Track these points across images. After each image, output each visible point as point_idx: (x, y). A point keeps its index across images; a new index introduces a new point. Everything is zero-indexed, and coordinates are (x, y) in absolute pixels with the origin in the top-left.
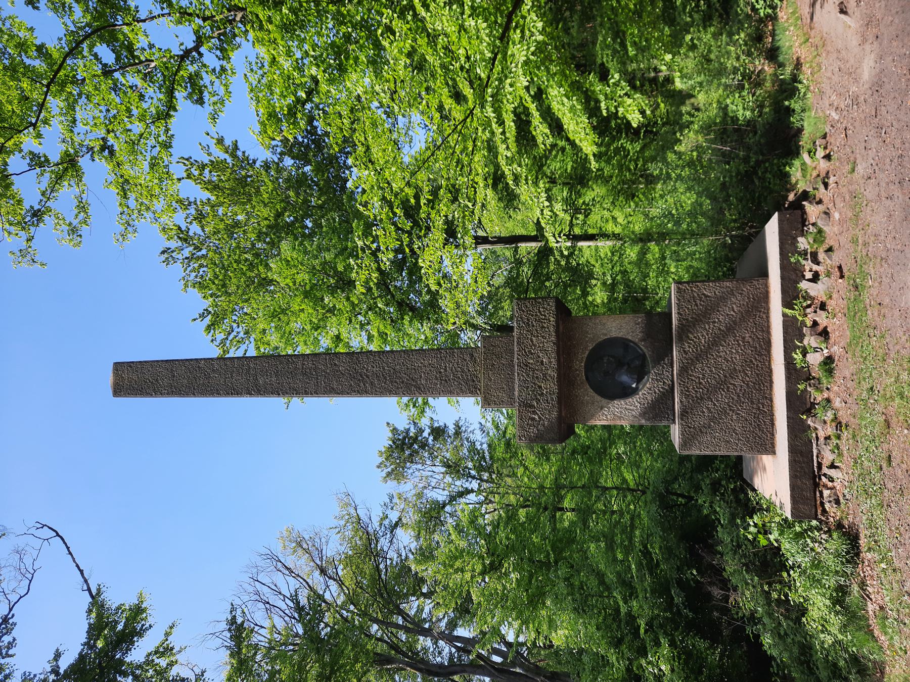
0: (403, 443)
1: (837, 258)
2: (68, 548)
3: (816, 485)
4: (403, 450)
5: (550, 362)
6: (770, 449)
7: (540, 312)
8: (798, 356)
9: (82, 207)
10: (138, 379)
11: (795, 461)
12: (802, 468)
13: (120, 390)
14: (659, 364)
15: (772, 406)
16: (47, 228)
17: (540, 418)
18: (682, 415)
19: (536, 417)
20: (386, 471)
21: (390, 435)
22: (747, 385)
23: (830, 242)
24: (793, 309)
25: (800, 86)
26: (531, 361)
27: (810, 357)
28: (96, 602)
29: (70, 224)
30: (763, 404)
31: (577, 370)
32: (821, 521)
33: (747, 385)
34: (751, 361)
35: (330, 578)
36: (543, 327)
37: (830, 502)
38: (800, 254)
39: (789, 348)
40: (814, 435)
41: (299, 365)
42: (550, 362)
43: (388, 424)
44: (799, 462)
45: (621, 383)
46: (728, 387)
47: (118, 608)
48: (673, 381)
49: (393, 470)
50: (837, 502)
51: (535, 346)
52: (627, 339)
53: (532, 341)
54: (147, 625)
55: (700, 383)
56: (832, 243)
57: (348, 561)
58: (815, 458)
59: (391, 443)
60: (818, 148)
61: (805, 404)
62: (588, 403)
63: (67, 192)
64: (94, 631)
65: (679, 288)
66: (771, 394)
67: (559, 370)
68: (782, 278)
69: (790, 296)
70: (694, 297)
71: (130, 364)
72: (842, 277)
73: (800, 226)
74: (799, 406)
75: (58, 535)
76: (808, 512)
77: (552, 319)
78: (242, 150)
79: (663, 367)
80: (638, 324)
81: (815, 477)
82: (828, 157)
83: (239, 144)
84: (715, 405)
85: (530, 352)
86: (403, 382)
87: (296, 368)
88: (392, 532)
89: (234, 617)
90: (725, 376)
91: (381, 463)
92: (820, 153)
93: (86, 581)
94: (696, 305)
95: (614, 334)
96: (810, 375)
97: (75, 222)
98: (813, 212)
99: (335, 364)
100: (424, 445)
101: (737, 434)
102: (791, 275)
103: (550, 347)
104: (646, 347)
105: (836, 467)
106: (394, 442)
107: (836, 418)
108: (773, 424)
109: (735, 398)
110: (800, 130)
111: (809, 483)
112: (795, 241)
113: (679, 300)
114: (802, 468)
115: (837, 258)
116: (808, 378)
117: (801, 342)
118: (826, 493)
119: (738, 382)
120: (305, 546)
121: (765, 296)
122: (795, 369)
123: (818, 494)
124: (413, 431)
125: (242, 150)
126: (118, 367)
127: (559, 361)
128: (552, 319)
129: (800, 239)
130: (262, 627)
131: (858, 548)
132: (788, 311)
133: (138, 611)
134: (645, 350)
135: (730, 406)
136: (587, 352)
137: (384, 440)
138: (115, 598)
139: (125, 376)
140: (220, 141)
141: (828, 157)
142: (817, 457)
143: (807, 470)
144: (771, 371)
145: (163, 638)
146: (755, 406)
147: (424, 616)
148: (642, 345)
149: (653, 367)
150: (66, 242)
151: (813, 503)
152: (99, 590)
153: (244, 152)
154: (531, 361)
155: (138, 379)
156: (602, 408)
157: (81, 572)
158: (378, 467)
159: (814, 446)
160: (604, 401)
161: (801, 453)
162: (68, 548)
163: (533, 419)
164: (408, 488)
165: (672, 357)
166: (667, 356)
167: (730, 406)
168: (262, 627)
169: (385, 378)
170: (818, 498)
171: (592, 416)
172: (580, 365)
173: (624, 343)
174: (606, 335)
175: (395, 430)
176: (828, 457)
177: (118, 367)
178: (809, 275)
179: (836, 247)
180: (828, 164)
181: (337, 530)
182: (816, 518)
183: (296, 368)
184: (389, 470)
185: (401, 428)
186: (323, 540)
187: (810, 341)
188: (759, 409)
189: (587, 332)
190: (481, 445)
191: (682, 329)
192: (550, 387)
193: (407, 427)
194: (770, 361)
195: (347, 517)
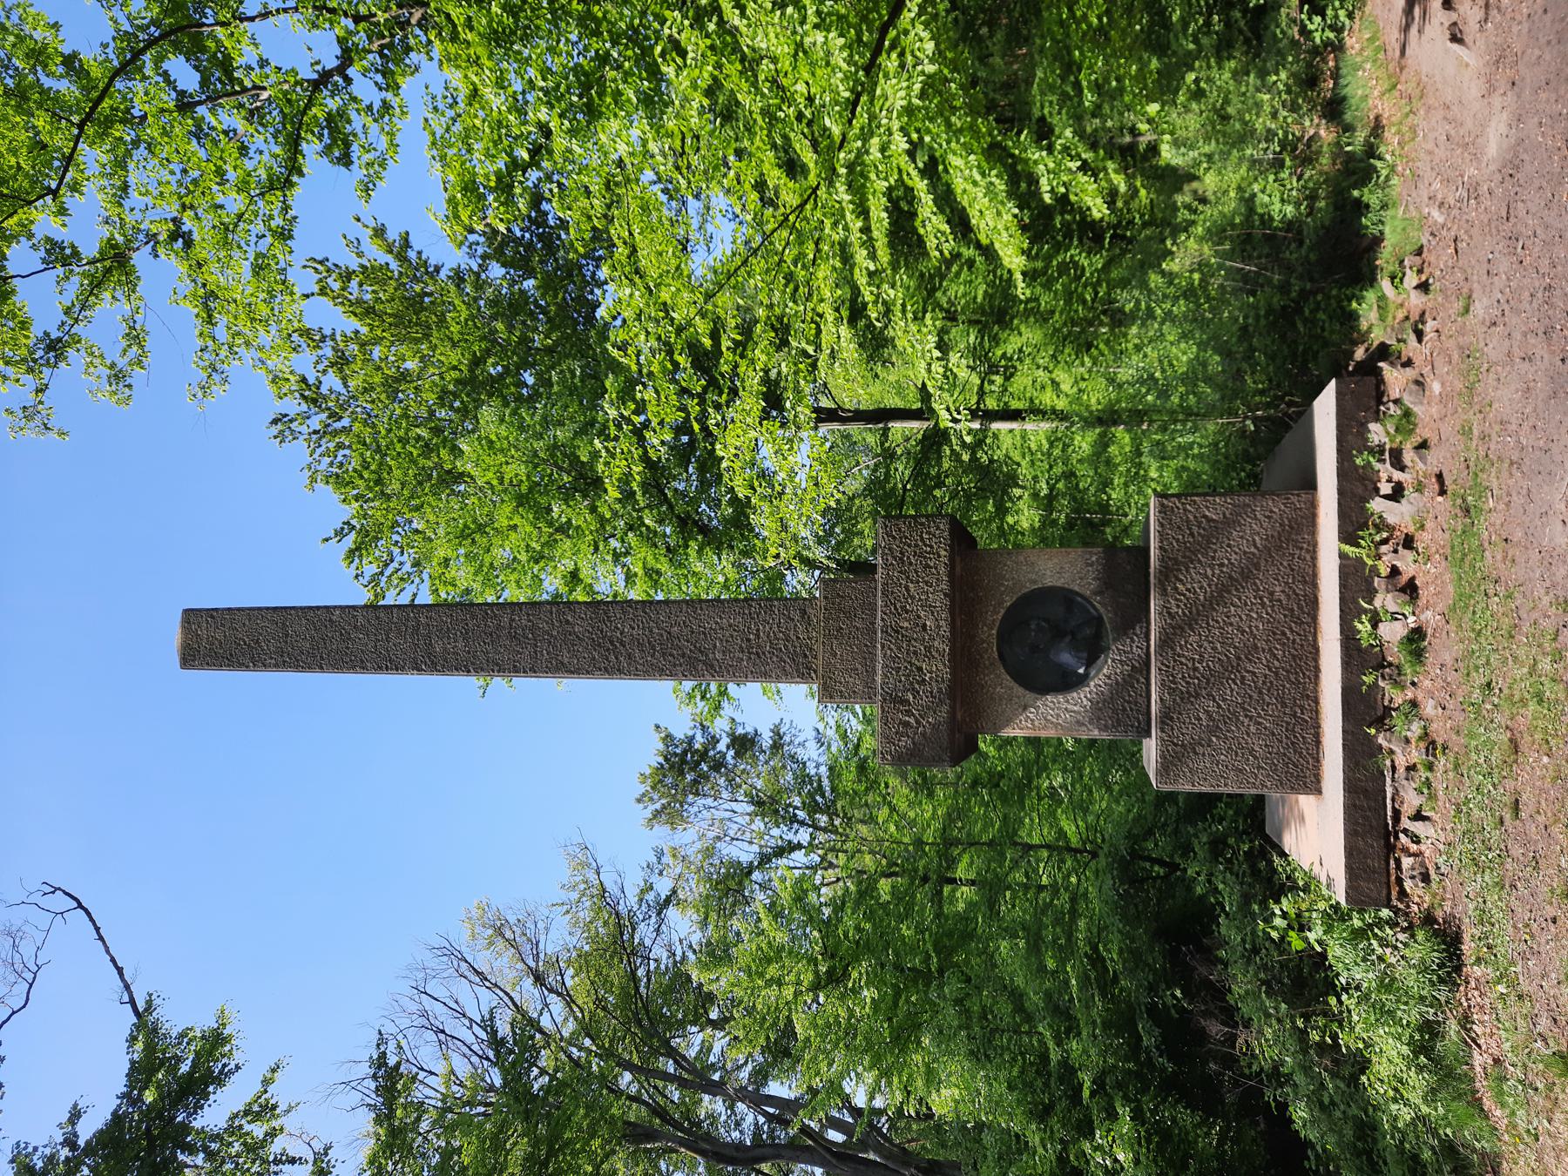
0: (683, 761)
2: (97, 929)
3: (1390, 848)
4: (682, 773)
5: (939, 627)
6: (1313, 786)
7: (922, 539)
8: (1363, 627)
9: (135, 337)
11: (1355, 806)
14: (1126, 634)
15: (1317, 712)
16: (72, 373)
17: (917, 722)
19: (912, 721)
21: (661, 746)
22: (1276, 674)
23: (1423, 432)
24: (1358, 546)
25: (1379, 164)
27: (1385, 629)
28: (145, 1024)
30: (1302, 708)
32: (1396, 911)
33: (1276, 674)
34: (1284, 634)
35: (551, 991)
36: (928, 566)
37: (1413, 877)
38: (1371, 451)
39: (1348, 613)
40: (1388, 763)
42: (939, 627)
43: (658, 727)
45: (1060, 665)
47: (182, 1035)
49: (664, 807)
50: (1426, 878)
51: (913, 598)
52: (1071, 591)
54: (232, 1066)
55: (1195, 669)
56: (1426, 434)
57: (583, 961)
58: (1388, 801)
59: (661, 759)
60: (1408, 271)
64: (140, 1074)
65: (1162, 505)
66: (1316, 691)
68: (1341, 492)
69: (1353, 524)
70: (1188, 521)
71: (212, 613)
72: (1442, 492)
73: (1373, 403)
74: (1364, 712)
75: (80, 905)
76: (1374, 895)
77: (943, 553)
81: (1389, 833)
82: (1424, 287)
83: (411, 238)
84: (1219, 706)
86: (683, 655)
87: (499, 627)
88: (659, 914)
90: (1239, 658)
91: (644, 795)
92: (1411, 279)
93: (127, 987)
94: (1192, 534)
95: (1049, 581)
96: (1384, 659)
97: (121, 362)
99: (567, 622)
100: (718, 765)
101: (1255, 758)
103: (939, 600)
106: (666, 759)
108: (1318, 743)
109: (1255, 696)
110: (1378, 240)
111: (1377, 845)
113: (1162, 525)
115: (1436, 459)
116: (1381, 664)
117: (1370, 603)
118: (1407, 862)
120: (508, 934)
122: (1359, 649)
125: (417, 248)
126: (192, 617)
127: (953, 625)
128: (943, 553)
129: (1373, 426)
130: (432, 1073)
132: (1348, 549)
133: (216, 1040)
134: (1102, 610)
137: (650, 755)
138: (176, 1017)
139: (203, 633)
140: (379, 232)
141: (1424, 287)
143: (1374, 823)
144: (1317, 650)
145: (259, 1088)
147: (712, 1059)
149: (1115, 640)
151: (1384, 880)
152: (149, 1003)
153: (419, 253)
156: (1025, 708)
157: (120, 971)
158: (639, 801)
159: (1388, 781)
160: (1029, 696)
162: (97, 929)
163: (907, 724)
168: (432, 1073)
170: (1393, 871)
171: (1008, 722)
172: (989, 634)
173: (1066, 597)
174: (1035, 582)
175: (668, 739)
176: (1412, 800)
177: (192, 617)
178: (1386, 488)
180: (1424, 298)
182: (1389, 906)
183: (499, 627)
184: (658, 806)
186: (541, 925)
188: (1295, 715)
190: (817, 767)
192: (937, 669)
193: (690, 733)
195: (583, 886)
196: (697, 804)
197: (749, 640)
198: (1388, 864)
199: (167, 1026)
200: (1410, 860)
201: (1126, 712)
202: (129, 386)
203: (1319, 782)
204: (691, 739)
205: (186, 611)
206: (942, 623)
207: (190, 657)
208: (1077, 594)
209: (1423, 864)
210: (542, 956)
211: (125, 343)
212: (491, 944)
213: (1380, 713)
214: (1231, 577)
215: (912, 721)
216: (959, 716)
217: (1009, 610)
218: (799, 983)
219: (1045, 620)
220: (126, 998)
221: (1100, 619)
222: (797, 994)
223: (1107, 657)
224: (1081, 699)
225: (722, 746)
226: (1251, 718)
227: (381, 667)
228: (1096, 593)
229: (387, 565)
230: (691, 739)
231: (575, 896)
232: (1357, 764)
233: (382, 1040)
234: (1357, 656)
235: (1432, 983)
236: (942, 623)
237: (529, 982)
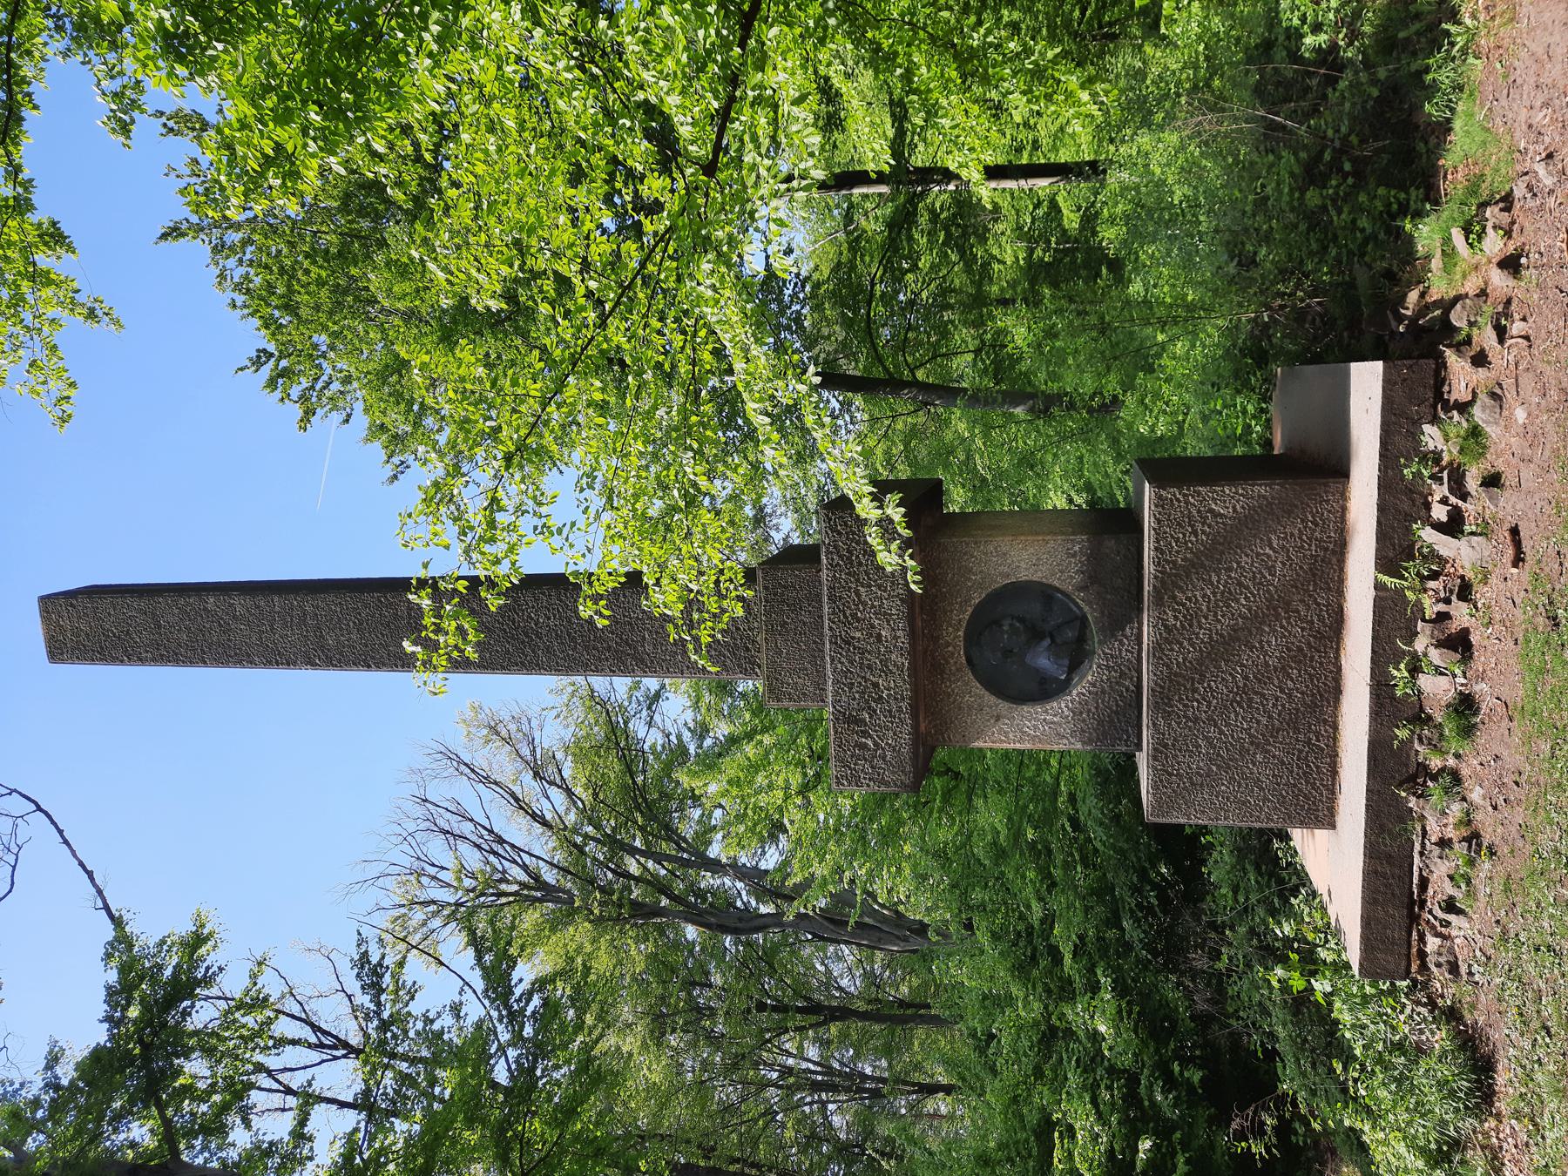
1: (1507, 506)
2: (60, 832)
3: (1414, 919)
5: (896, 638)
6: (1323, 815)
8: (1400, 673)
10: (102, 624)
11: (1376, 872)
13: (61, 648)
14: (1113, 635)
15: (1335, 739)
17: (876, 744)
19: (870, 743)
22: (1290, 696)
23: (1496, 460)
24: (1402, 578)
25: (1453, 29)
26: (858, 634)
27: (1426, 682)
28: (122, 940)
30: (1318, 734)
33: (1290, 696)
35: (552, 783)
37: (1439, 965)
38: (1424, 458)
40: (1419, 828)
42: (896, 638)
44: (1384, 875)
45: (1037, 670)
46: (1250, 700)
47: (163, 942)
50: (1454, 968)
51: (865, 604)
52: (1050, 586)
54: (215, 969)
56: (1500, 466)
57: (580, 752)
60: (1489, 230)
61: (1407, 765)
62: (970, 708)
64: (117, 996)
65: (1160, 497)
66: (1335, 716)
67: (912, 653)
68: (1382, 508)
69: (1395, 551)
72: (1518, 560)
73: (1430, 394)
74: (1395, 774)
75: (39, 808)
76: (1392, 967)
80: (1074, 556)
81: (1413, 903)
82: (1511, 264)
84: (1221, 732)
85: (854, 616)
88: (649, 708)
89: (365, 956)
90: (1246, 678)
92: (1494, 244)
93: (100, 892)
94: (1195, 533)
95: (1024, 575)
96: (1422, 709)
98: (1461, 376)
101: (1261, 789)
102: (1400, 506)
104: (1089, 603)
105: (1459, 912)
107: (1469, 822)
108: (1334, 773)
110: (1445, 127)
111: (1399, 914)
112: (1415, 435)
113: (1159, 521)
115: (1507, 506)
116: (1419, 717)
118: (1432, 943)
119: (1270, 691)
120: (504, 733)
121: (1339, 548)
122: (1393, 697)
126: (49, 604)
127: (912, 635)
129: (1427, 428)
130: (443, 868)
131: (1490, 1086)
132: (1388, 580)
133: (197, 941)
134: (1087, 609)
135: (1251, 736)
136: (970, 610)
138: (148, 930)
141: (1511, 264)
144: (1339, 669)
145: (247, 982)
146: (1301, 737)
147: (713, 822)
148: (1079, 597)
154: (858, 634)
155: (102, 624)
156: (998, 718)
157: (90, 874)
159: (1417, 847)
160: (1003, 706)
161: (1389, 857)
162: (60, 832)
163: (864, 747)
166: (1131, 621)
167: (1251, 736)
168: (443, 868)
169: (573, 639)
170: (1415, 943)
171: (979, 735)
172: (955, 636)
176: (1442, 886)
177: (49, 604)
178: (1440, 513)
179: (1509, 478)
180: (1511, 282)
181: (555, 713)
186: (534, 723)
188: (1309, 742)
191: (1163, 582)
192: (895, 685)
194: (1338, 651)
198: (1410, 935)
199: (143, 937)
200: (1438, 941)
201: (1116, 721)
206: (900, 633)
208: (1058, 590)
209: (1451, 951)
210: (538, 751)
212: (488, 742)
214: (1240, 584)
215: (870, 743)
218: (787, 788)
219: (1022, 620)
222: (787, 798)
223: (1091, 661)
224: (1060, 709)
227: (269, 663)
229: (316, 379)
232: (1382, 828)
233: (361, 941)
234: (1388, 706)
235: (1457, 1110)
236: (900, 633)
237: (528, 777)
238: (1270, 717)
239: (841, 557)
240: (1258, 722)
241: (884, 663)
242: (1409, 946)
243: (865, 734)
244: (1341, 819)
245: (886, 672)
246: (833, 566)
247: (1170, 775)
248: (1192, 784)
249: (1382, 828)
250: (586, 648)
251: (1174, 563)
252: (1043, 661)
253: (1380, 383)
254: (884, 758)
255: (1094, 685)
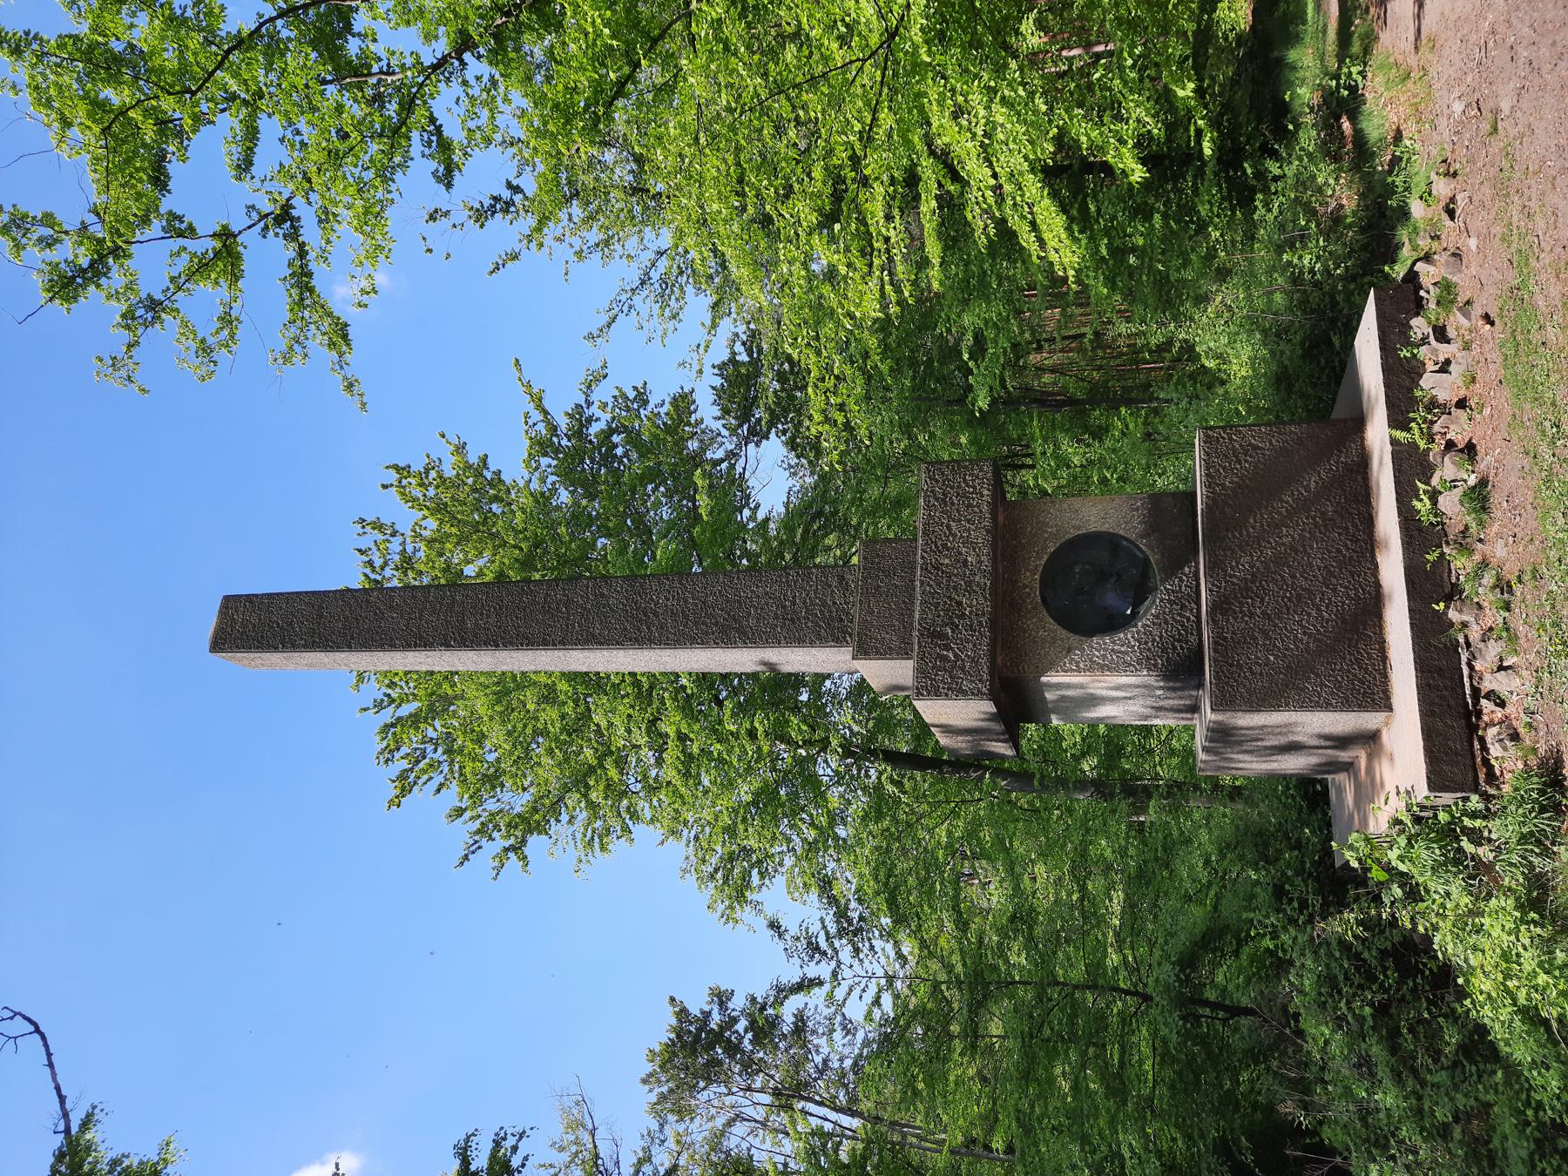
0: (697, 1039)
2: (49, 1055)
3: (1472, 729)
4: (694, 1052)
7: (965, 481)
8: (1422, 506)
9: (227, 320)
11: (1429, 685)
12: (1442, 697)
16: (163, 337)
17: (956, 655)
18: (1215, 643)
20: (657, 1090)
21: (674, 1021)
22: (1334, 590)
24: (1409, 430)
29: (203, 341)
31: (1025, 586)
32: (1487, 798)
33: (1334, 590)
34: (1339, 551)
39: (1405, 494)
41: (540, 598)
42: (980, 562)
43: (672, 999)
44: (1437, 688)
48: (1199, 617)
49: (671, 1091)
51: (954, 536)
53: (949, 527)
58: (1466, 679)
59: (673, 1036)
63: (208, 296)
65: (1207, 436)
69: (1401, 407)
70: (1234, 449)
71: (250, 598)
74: (1430, 587)
75: (37, 1030)
76: (1460, 778)
78: (493, 468)
79: (1181, 580)
81: (1468, 714)
84: (1276, 625)
86: (716, 624)
87: (533, 603)
91: (651, 1075)
97: (211, 341)
99: (602, 595)
100: (733, 1049)
103: (980, 537)
104: (1150, 547)
106: (679, 1036)
108: (1384, 658)
111: (1458, 725)
113: (1207, 454)
114: (1442, 697)
117: (1428, 484)
123: (1477, 745)
124: (716, 1017)
125: (493, 468)
127: (994, 561)
129: (1415, 322)
134: (1148, 552)
135: (1303, 627)
136: (1046, 557)
137: (661, 1031)
139: (238, 618)
140: (461, 449)
142: (1471, 677)
143: (1452, 703)
144: (1377, 566)
149: (1163, 581)
150: (193, 366)
151: (1469, 762)
152: (86, 1124)
157: (62, 1099)
158: (644, 1081)
160: (1074, 639)
161: (1440, 671)
162: (49, 1055)
163: (945, 659)
164: (699, 1130)
165: (1197, 563)
167: (1303, 627)
169: (686, 617)
171: (1050, 666)
172: (1031, 578)
173: (1111, 542)
174: (1079, 528)
175: (683, 1013)
177: (230, 603)
180: (1453, 184)
182: (1476, 790)
183: (533, 603)
184: (665, 1089)
185: (695, 1010)
187: (1448, 469)
189: (1047, 525)
190: (841, 1060)
192: (977, 603)
193: (707, 1008)
195: (574, 1149)
196: (709, 1094)
197: (784, 607)
198: (1472, 745)
202: (215, 363)
203: (1388, 698)
204: (707, 1015)
205: (227, 599)
207: (224, 641)
209: (1510, 726)
211: (219, 325)
213: (1447, 590)
216: (999, 660)
217: (1053, 555)
220: (61, 1127)
221: (1147, 559)
225: (741, 1026)
226: (1310, 636)
228: (1143, 537)
229: (418, 762)
230: (707, 1015)
231: (565, 1157)
234: (1418, 536)
238: (1319, 610)
239: (937, 499)
240: (1309, 615)
241: (969, 583)
242: (1473, 757)
243: (947, 648)
244: (1396, 701)
245: (969, 591)
246: (928, 506)
247: (1231, 665)
248: (1253, 673)
249: (1433, 713)
250: (696, 624)
251: (1223, 485)
252: (1111, 598)
253: (1412, 656)
254: (963, 669)
255: (1157, 617)
